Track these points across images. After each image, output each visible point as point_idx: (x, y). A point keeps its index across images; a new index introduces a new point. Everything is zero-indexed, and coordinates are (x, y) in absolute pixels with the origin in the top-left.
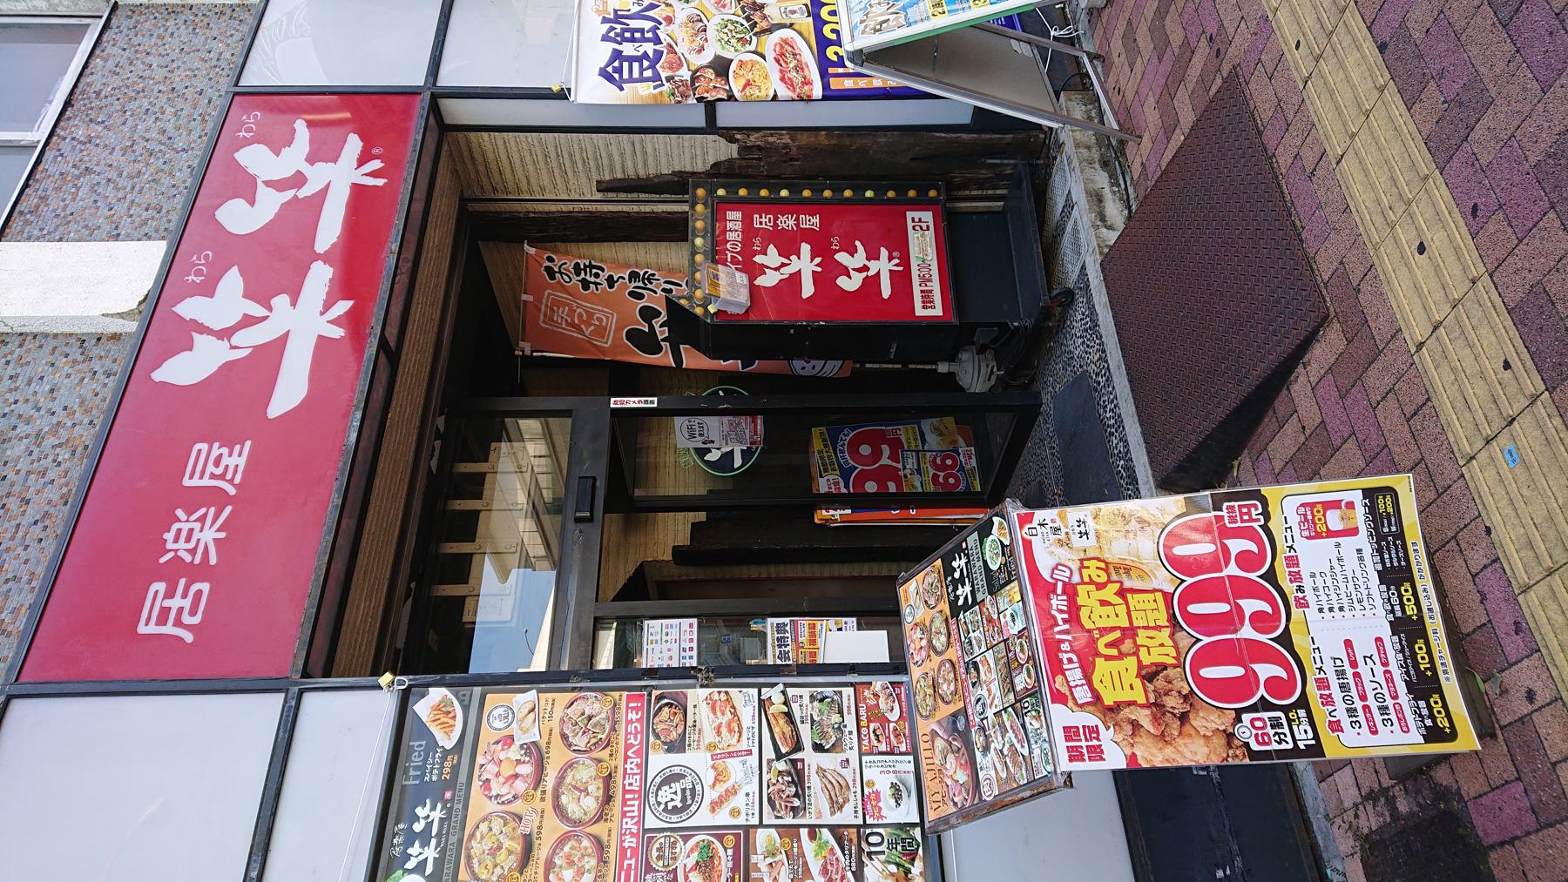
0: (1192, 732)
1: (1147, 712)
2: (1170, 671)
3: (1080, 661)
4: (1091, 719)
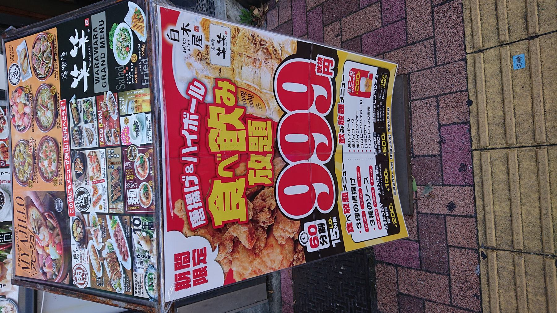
0: (274, 242)
1: (246, 228)
2: (267, 191)
3: (200, 184)
4: (200, 242)
